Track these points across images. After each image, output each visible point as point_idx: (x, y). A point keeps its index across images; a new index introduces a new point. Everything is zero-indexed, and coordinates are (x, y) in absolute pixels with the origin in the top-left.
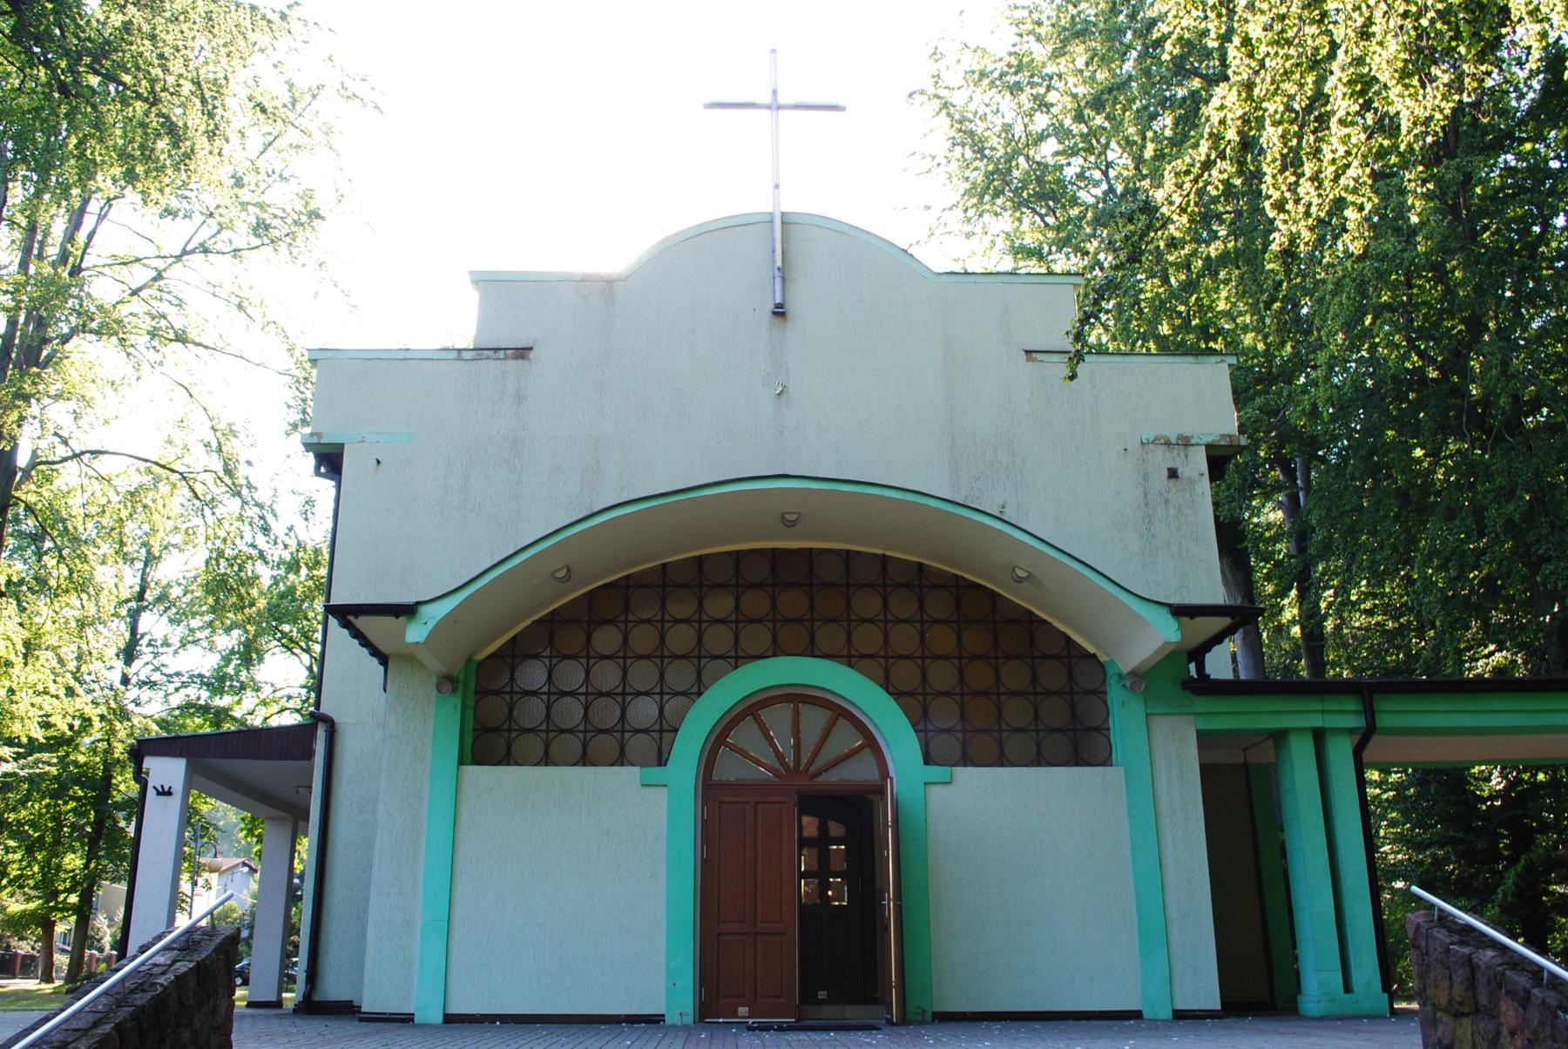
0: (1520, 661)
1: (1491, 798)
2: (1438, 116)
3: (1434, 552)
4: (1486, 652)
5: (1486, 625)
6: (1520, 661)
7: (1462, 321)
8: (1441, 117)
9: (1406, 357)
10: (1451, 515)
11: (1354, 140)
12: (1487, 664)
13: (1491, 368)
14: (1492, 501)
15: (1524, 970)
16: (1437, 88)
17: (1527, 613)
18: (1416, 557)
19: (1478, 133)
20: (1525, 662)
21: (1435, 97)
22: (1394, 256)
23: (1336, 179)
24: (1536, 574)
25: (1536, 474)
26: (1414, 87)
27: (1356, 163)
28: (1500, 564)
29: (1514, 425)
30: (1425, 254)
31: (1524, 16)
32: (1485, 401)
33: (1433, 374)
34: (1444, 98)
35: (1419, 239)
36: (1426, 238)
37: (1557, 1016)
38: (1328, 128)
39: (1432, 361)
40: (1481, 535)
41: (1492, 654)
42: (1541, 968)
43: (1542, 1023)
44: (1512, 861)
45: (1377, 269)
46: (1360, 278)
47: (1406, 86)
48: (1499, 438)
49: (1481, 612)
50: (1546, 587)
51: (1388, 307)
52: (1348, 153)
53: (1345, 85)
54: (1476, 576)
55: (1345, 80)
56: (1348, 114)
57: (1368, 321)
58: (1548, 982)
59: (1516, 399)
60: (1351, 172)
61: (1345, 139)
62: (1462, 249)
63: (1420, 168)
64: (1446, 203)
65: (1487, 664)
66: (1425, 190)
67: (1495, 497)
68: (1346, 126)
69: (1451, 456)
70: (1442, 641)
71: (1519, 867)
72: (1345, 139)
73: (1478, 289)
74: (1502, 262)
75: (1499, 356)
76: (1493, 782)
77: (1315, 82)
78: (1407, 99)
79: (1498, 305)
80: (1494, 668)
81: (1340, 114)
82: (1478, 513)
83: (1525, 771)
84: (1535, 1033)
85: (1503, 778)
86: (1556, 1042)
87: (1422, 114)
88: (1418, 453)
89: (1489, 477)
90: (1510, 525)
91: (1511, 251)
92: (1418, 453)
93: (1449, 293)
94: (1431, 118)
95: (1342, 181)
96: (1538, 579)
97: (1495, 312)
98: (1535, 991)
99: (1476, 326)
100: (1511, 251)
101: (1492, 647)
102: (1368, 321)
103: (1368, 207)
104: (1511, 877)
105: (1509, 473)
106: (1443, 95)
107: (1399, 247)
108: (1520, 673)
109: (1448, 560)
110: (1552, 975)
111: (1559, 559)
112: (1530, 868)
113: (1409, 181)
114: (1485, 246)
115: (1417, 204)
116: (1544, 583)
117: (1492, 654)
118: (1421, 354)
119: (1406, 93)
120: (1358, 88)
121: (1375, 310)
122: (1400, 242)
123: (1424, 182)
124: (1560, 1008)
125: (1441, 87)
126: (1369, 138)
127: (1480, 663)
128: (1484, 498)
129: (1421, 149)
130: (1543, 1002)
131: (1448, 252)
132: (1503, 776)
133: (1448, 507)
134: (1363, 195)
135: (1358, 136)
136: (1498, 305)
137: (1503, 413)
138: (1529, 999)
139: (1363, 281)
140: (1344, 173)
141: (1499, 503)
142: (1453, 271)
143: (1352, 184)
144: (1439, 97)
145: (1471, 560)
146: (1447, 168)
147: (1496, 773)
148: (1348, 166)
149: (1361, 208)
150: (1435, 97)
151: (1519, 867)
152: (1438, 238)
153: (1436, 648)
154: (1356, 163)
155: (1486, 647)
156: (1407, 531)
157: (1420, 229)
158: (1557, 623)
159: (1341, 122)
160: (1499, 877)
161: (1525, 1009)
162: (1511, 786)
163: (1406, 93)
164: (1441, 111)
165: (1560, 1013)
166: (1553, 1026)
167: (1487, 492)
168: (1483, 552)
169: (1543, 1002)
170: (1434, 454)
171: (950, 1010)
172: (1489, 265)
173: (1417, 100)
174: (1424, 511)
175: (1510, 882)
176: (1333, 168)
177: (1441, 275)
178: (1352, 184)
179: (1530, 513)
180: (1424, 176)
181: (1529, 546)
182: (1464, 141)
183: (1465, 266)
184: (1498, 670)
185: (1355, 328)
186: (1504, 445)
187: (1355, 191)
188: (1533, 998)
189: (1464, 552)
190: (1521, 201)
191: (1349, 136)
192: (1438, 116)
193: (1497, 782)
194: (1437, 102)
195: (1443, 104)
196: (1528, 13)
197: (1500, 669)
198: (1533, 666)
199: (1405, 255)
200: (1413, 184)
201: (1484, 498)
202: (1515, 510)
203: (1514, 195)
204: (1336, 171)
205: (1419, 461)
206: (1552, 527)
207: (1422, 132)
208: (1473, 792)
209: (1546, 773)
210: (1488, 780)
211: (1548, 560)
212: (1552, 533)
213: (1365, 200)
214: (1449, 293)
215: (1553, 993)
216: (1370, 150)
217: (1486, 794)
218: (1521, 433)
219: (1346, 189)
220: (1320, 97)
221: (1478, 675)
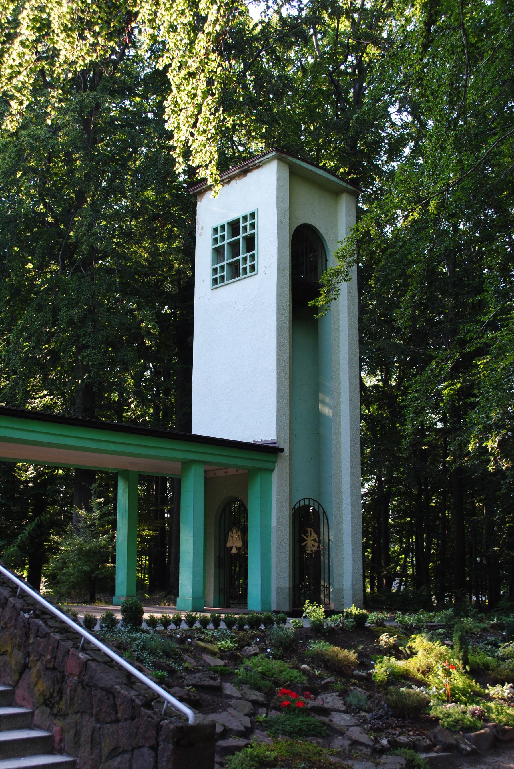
0: (59, 403)
1: (27, 481)
2: (81, 62)
3: (24, 329)
4: (42, 394)
5: (45, 379)
6: (59, 403)
7: (74, 192)
8: (83, 64)
9: (37, 204)
10: (39, 309)
11: (27, 57)
12: (41, 402)
13: (83, 226)
14: (65, 306)
15: (8, 586)
16: (85, 44)
17: (69, 376)
18: (13, 329)
19: (112, 81)
20: (62, 404)
21: (82, 50)
22: (44, 139)
23: (10, 79)
24: (79, 354)
25: (93, 295)
26: (73, 38)
27: (25, 73)
28: (61, 344)
29: (87, 263)
30: (62, 144)
31: (146, 21)
32: (77, 244)
33: (50, 220)
34: (88, 53)
35: (61, 133)
36: (65, 135)
37: (19, 614)
38: (13, 43)
39: (53, 212)
40: (54, 324)
41: (44, 396)
42: (17, 586)
43: (10, 618)
44: (31, 519)
45: (31, 144)
46: (19, 146)
47: (69, 36)
48: (77, 269)
49: (43, 368)
50: (82, 363)
51: (34, 170)
52: (21, 65)
53: (30, 20)
54: (46, 348)
55: (31, 17)
56: (27, 39)
57: (19, 174)
58: (20, 594)
59: (92, 248)
60: (21, 77)
61: (21, 55)
62: (85, 148)
63: (60, 92)
64: (83, 117)
65: (41, 402)
66: (60, 106)
67: (67, 304)
68: (24, 47)
69: (51, 272)
70: (17, 384)
71: (33, 524)
72: (21, 55)
73: (87, 175)
74: (105, 163)
75: (89, 220)
76: (29, 473)
77: (14, 10)
78: (67, 44)
79: (96, 190)
80: (44, 405)
81: (23, 38)
82: (55, 311)
83: (48, 468)
84: (6, 624)
85: (35, 471)
86: (16, 629)
87: (72, 58)
88: (30, 266)
89: (65, 291)
90: (71, 322)
91: (112, 159)
92: (30, 266)
93: (70, 173)
94: (75, 63)
95: (14, 81)
96: (79, 357)
97: (94, 193)
98: (11, 599)
99: (81, 197)
100: (112, 159)
101: (45, 392)
102: (19, 174)
103: (26, 103)
104: (29, 528)
105: (78, 291)
106: (88, 50)
107: (48, 135)
108: (57, 411)
109: (31, 336)
110: (23, 591)
111: (94, 348)
112: (39, 525)
113: (53, 97)
114: (98, 151)
115: (53, 113)
116: (82, 361)
117: (44, 396)
118: (46, 205)
119: (68, 40)
120: (38, 25)
121: (23, 169)
122: (49, 132)
123: (60, 101)
124: (22, 609)
125: (88, 45)
126: (37, 60)
127: (37, 400)
128: (61, 303)
129: (64, 80)
130: (14, 606)
131: (77, 149)
132: (35, 470)
133: (39, 303)
134: (24, 95)
135: (29, 56)
136: (96, 190)
137: (83, 255)
138: (6, 603)
139: (21, 149)
140: (16, 76)
141: (68, 308)
142: (77, 159)
143: (20, 85)
144: (85, 51)
145: (45, 338)
146: (88, 96)
147: (32, 467)
148: (19, 73)
149: (21, 103)
150: (82, 50)
151: (33, 524)
152: (71, 137)
153: (13, 388)
154: (25, 73)
155: (43, 391)
156: (12, 312)
157: (63, 128)
158: (84, 385)
159: (22, 43)
160: (22, 527)
161: (3, 609)
162: (39, 475)
163: (68, 40)
164: (84, 59)
165: (22, 613)
166: (16, 619)
167: (64, 299)
168: (53, 334)
169: (14, 606)
170: (41, 267)
171: (181, 536)
172: (97, 163)
173: (72, 47)
174: (25, 302)
175: (26, 532)
176: (10, 71)
177: (69, 161)
178: (20, 85)
179: (83, 320)
180: (61, 97)
181: (79, 337)
182: (103, 82)
183: (83, 159)
184: (46, 407)
185: (10, 177)
186: (79, 274)
187: (19, 90)
188: (9, 604)
189: (42, 332)
190: (125, 131)
191: (24, 54)
192: (81, 62)
193: (31, 473)
194: (83, 54)
195: (86, 56)
196: (148, 20)
197: (47, 406)
198: (66, 408)
199: (50, 141)
200: (54, 100)
201: (61, 303)
202: (76, 314)
203: (122, 126)
204: (11, 74)
205: (29, 271)
206: (94, 329)
207: (67, 69)
208: (16, 477)
209: (63, 471)
210: (26, 471)
211: (87, 347)
212: (93, 332)
213: (25, 99)
214: (70, 173)
215: (20, 601)
216: (36, 68)
217: (23, 479)
218: (90, 268)
219: (16, 87)
220: (15, 23)
221: (33, 408)
